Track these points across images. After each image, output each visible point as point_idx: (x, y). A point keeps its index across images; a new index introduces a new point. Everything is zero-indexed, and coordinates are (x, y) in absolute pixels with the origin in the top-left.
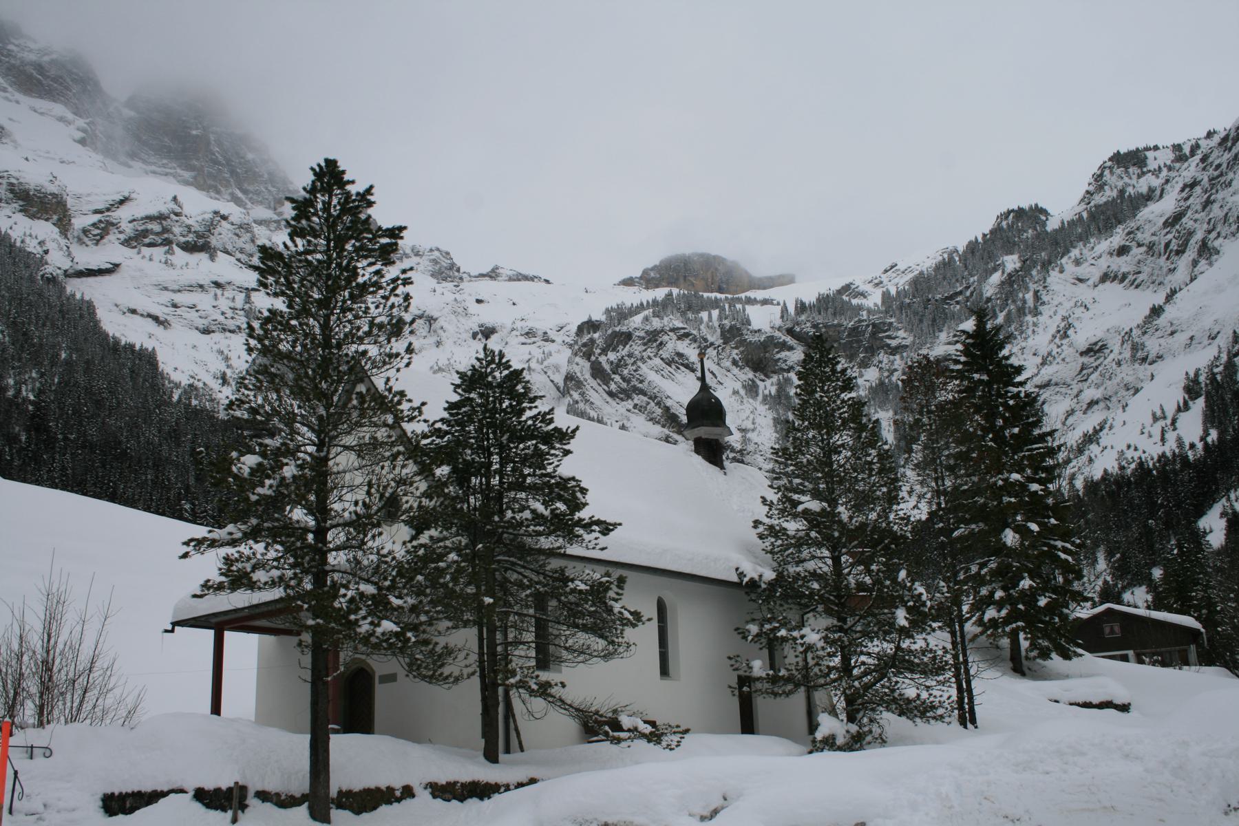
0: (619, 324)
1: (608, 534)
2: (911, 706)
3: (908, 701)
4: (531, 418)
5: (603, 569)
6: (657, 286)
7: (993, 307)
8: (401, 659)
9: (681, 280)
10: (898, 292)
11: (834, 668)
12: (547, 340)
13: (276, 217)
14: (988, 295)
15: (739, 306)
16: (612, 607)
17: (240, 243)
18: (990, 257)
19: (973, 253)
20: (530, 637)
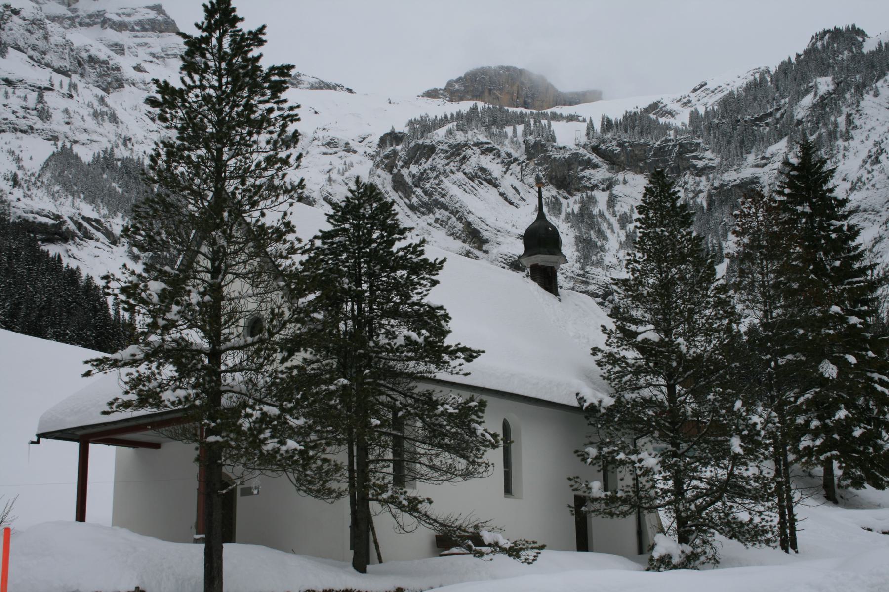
0: (422, 136)
1: (471, 361)
2: (743, 530)
3: (742, 524)
4: (402, 249)
5: (467, 395)
6: (461, 99)
7: (803, 130)
8: (291, 475)
9: (487, 93)
10: (707, 113)
11: (668, 491)
12: (348, 151)
13: (70, 14)
14: (799, 117)
15: (544, 122)
16: (475, 429)
17: (32, 40)
18: (802, 79)
19: (785, 73)
20: (389, 455)
